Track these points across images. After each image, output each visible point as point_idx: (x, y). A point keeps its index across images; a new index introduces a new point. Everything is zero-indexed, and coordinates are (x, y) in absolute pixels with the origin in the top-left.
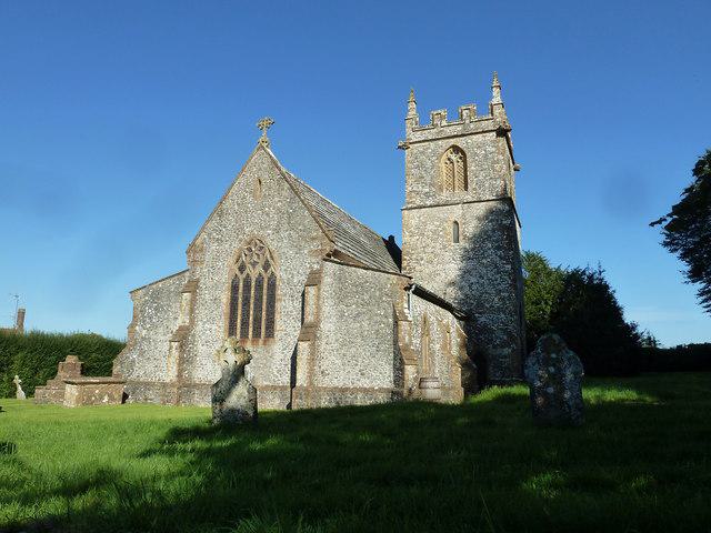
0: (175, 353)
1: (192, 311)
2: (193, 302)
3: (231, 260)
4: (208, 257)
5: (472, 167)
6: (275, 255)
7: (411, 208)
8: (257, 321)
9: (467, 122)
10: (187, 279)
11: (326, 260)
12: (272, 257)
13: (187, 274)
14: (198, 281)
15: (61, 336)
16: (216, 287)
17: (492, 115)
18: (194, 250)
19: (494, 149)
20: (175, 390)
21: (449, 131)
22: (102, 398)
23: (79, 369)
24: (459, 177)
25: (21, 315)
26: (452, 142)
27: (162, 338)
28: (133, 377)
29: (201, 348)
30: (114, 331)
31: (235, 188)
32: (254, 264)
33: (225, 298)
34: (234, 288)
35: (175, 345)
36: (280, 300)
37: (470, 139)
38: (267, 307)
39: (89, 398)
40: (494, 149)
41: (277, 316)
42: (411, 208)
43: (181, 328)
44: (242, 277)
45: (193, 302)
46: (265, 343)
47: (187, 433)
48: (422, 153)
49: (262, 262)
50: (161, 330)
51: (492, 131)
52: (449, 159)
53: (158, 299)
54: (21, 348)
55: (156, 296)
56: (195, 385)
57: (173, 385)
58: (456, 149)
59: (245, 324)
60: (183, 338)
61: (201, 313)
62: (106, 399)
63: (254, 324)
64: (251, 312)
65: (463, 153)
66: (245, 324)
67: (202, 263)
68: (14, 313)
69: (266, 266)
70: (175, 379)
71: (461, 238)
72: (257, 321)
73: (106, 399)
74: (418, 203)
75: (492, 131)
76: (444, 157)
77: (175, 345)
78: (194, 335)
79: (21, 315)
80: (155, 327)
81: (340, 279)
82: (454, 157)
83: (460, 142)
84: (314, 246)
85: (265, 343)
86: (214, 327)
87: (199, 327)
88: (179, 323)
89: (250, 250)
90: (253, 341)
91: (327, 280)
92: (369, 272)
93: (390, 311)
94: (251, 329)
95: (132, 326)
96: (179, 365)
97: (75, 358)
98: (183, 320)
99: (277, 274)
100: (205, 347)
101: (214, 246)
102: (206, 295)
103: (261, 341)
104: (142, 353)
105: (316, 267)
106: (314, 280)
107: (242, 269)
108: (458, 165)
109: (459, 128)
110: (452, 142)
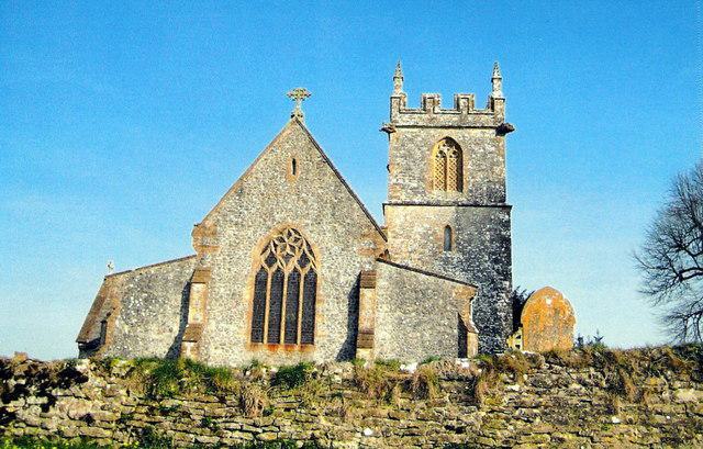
3: (256, 251)
4: (223, 243)
5: (468, 166)
6: (315, 250)
7: (397, 204)
9: (465, 112)
10: (193, 267)
11: (378, 260)
12: (311, 252)
13: (193, 261)
14: (208, 270)
17: (493, 108)
18: (204, 233)
19: (493, 149)
21: (443, 119)
24: (452, 174)
26: (447, 133)
27: (155, 336)
31: (261, 164)
32: (287, 258)
33: (248, 294)
34: (260, 282)
36: (322, 301)
37: (466, 133)
40: (493, 149)
41: (318, 320)
42: (397, 204)
44: (271, 271)
48: (411, 140)
49: (298, 255)
50: (154, 327)
51: (491, 128)
52: (441, 152)
58: (450, 141)
59: (275, 326)
65: (458, 147)
66: (275, 326)
67: (215, 249)
69: (304, 260)
71: (454, 245)
74: (404, 198)
75: (491, 128)
76: (436, 150)
80: (143, 321)
81: (400, 284)
82: (447, 150)
83: (455, 134)
84: (366, 243)
87: (212, 326)
89: (282, 240)
90: (286, 347)
91: (381, 283)
92: (432, 279)
93: (456, 322)
99: (318, 271)
101: (231, 230)
105: (368, 267)
106: (362, 282)
107: (271, 260)
108: (452, 161)
109: (456, 118)
110: (447, 133)
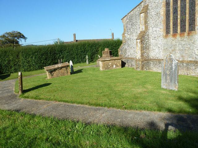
0: (139, 45)
1: (146, 22)
2: (146, 18)
8: (183, 21)
13: (142, 4)
14: (148, 5)
15: (36, 46)
16: (157, 7)
20: (140, 63)
22: (112, 66)
23: (109, 53)
25: (113, 34)
28: (127, 56)
29: (152, 41)
30: (118, 36)
33: (162, 11)
35: (139, 41)
38: (190, 11)
39: (107, 66)
43: (141, 32)
45: (146, 18)
46: (189, 34)
47: (167, 24)
53: (132, 20)
54: (101, 46)
55: (131, 19)
56: (151, 60)
57: (139, 60)
59: (175, 24)
60: (143, 37)
61: (151, 22)
62: (114, 66)
63: (181, 24)
64: (179, 17)
68: (111, 34)
70: (140, 58)
72: (183, 21)
73: (114, 66)
77: (139, 41)
78: (148, 35)
79: (113, 34)
85: (189, 34)
86: (158, 29)
87: (150, 30)
88: (141, 30)
90: (180, 35)
94: (179, 27)
95: (124, 34)
96: (141, 50)
97: (107, 49)
98: (142, 28)
100: (154, 40)
102: (152, 12)
103: (186, 34)
104: (128, 46)
